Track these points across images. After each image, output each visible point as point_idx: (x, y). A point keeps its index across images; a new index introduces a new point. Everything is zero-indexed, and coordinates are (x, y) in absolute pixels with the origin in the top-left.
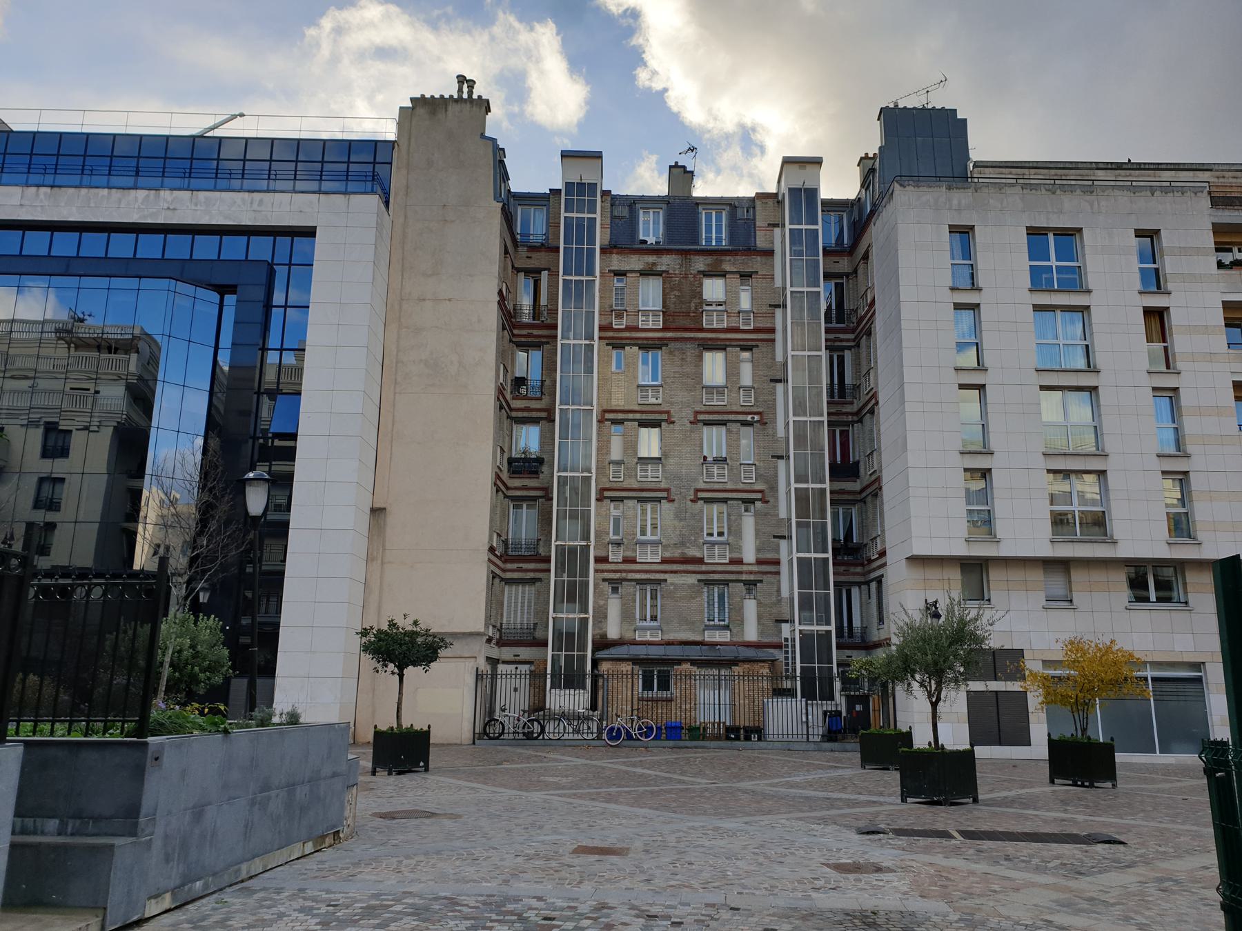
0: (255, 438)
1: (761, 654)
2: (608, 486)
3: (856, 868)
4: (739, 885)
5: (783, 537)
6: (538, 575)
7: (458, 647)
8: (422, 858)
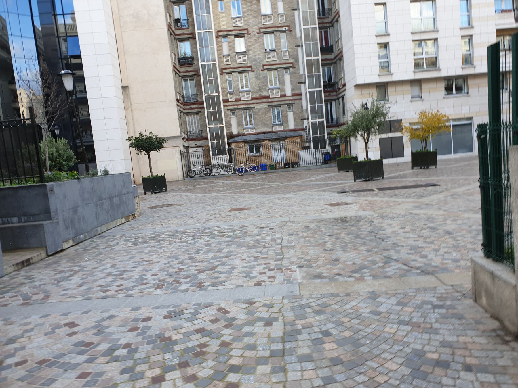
1: (297, 133)
2: (224, 67)
3: (338, 204)
5: (302, 83)
6: (199, 110)
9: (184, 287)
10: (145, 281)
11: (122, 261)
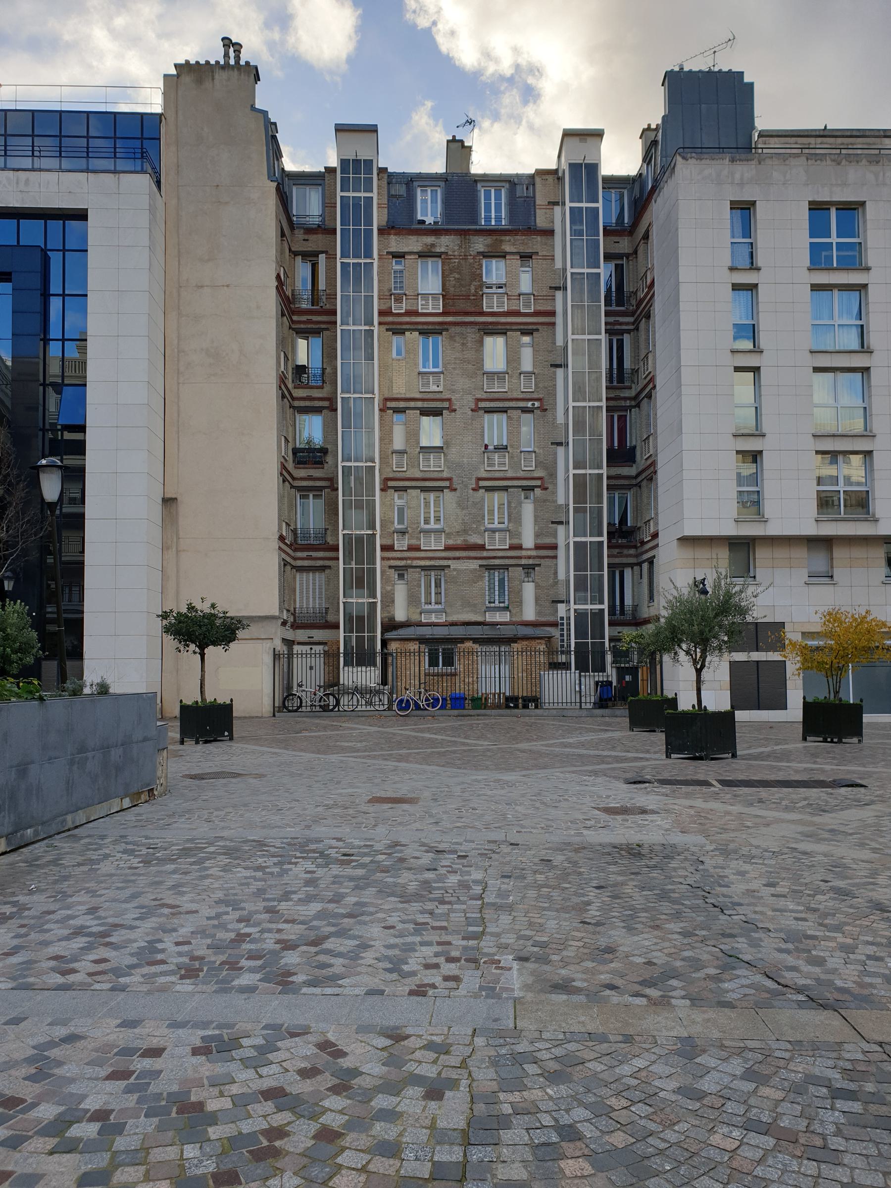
0: (44, 430)
1: (539, 632)
2: (391, 475)
3: (624, 811)
4: (518, 825)
5: (561, 523)
6: (327, 563)
7: (254, 630)
8: (230, 810)
9: (246, 979)
10: (159, 957)
11: (114, 900)
